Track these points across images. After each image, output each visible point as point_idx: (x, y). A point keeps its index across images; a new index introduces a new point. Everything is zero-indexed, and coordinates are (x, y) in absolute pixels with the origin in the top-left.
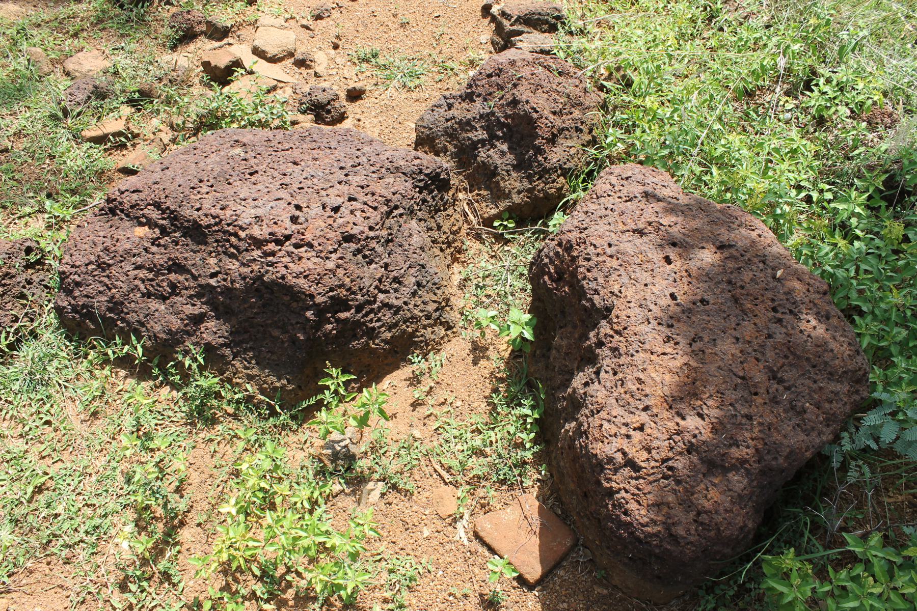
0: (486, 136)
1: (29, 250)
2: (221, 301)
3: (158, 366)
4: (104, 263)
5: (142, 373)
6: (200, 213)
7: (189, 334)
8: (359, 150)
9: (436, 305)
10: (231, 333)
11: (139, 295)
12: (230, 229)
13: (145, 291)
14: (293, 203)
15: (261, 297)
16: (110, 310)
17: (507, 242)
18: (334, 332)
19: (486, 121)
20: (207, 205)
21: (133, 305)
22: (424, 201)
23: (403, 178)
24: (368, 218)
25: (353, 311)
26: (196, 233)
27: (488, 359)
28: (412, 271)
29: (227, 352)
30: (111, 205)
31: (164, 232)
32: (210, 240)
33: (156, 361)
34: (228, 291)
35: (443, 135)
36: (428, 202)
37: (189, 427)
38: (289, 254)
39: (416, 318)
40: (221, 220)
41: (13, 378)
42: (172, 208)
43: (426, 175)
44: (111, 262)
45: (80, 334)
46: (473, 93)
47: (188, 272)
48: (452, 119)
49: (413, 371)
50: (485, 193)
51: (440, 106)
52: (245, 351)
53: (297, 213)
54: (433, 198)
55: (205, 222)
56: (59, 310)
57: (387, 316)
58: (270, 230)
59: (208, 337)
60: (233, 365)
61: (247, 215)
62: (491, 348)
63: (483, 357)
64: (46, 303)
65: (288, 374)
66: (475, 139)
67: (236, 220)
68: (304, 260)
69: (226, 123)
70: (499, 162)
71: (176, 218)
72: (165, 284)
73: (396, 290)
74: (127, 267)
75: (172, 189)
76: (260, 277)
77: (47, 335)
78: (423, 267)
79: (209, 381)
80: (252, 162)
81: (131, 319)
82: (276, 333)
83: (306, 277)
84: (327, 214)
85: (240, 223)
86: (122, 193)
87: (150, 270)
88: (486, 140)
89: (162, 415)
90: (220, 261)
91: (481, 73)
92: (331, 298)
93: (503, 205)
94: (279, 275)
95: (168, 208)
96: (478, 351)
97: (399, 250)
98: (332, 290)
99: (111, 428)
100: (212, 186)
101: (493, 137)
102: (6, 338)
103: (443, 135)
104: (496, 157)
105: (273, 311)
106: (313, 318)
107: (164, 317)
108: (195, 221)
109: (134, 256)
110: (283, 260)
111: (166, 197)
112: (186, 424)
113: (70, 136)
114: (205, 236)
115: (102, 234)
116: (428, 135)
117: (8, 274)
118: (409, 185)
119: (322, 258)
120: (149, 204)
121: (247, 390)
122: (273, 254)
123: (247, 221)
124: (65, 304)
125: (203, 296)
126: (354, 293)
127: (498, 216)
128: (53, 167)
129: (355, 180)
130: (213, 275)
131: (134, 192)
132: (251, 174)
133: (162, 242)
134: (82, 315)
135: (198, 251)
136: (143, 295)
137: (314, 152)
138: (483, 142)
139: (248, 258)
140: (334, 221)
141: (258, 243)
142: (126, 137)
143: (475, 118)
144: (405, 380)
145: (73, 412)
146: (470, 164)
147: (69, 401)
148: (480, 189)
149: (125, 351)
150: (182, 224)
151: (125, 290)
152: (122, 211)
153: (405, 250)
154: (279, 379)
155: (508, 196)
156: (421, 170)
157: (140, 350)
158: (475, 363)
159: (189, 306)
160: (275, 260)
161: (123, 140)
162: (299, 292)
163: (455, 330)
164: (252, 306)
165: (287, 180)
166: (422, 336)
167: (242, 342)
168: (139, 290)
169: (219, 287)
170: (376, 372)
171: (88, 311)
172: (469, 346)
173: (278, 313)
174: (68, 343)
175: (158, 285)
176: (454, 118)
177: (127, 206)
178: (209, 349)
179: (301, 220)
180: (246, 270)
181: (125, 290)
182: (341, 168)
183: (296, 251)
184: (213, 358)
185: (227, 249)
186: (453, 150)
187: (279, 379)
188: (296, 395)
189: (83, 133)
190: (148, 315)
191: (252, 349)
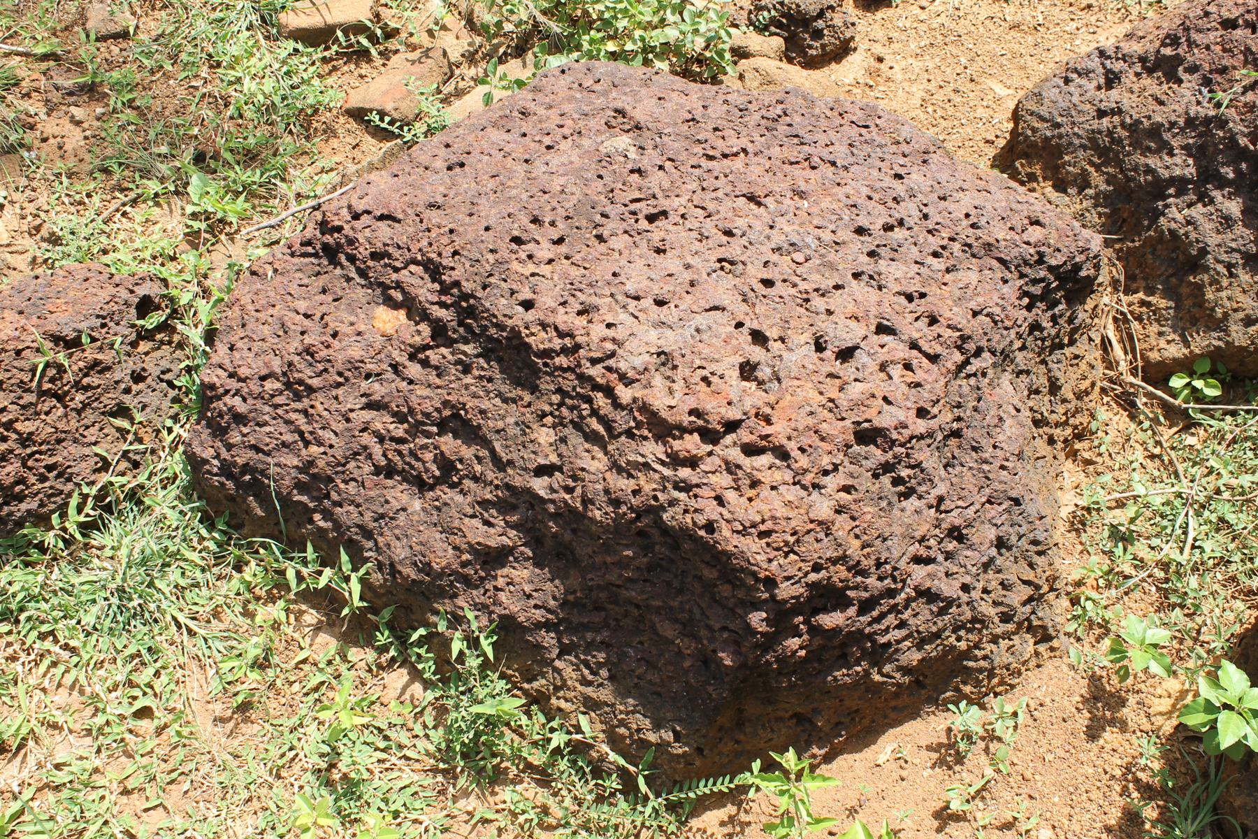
0: (1190, 172)
1: (145, 306)
2: (554, 534)
3: (391, 626)
4: (301, 382)
5: (357, 631)
6: (531, 316)
7: (467, 582)
8: (898, 176)
9: (1029, 591)
10: (564, 604)
11: (368, 468)
12: (596, 372)
13: (383, 463)
14: (748, 324)
15: (647, 549)
16: (301, 487)
17: (1189, 425)
18: (803, 653)
19: (1200, 135)
20: (547, 300)
21: (352, 488)
22: (1035, 327)
23: (1000, 272)
24: (918, 385)
25: (852, 611)
26: (515, 358)
27: (1123, 726)
28: (992, 511)
29: (548, 639)
30: (328, 239)
31: (440, 333)
32: (546, 384)
33: (386, 614)
34: (573, 518)
35: (1084, 147)
36: (1041, 329)
37: (440, 778)
38: (731, 468)
39: (982, 622)
40: (577, 347)
41: (84, 598)
42: (467, 286)
43: (1051, 269)
44: (315, 382)
45: (233, 515)
46: (1178, 60)
47: (486, 443)
48: (1113, 112)
49: (949, 730)
50: (1163, 303)
51: (1085, 73)
52: (589, 647)
53: (757, 354)
54: (1054, 319)
55: (540, 340)
56: (195, 463)
57: (921, 617)
58: (692, 403)
59: (510, 603)
60: (557, 670)
61: (640, 343)
62: (1132, 700)
63: (1112, 722)
64: (169, 423)
65: (680, 721)
66: (1165, 174)
67: (613, 354)
68: (765, 492)
69: (592, 42)
70: (1213, 240)
71: (471, 312)
72: (429, 456)
73: (949, 556)
74: (351, 400)
75: (471, 236)
76: (654, 511)
77: (164, 502)
78: (1017, 502)
79: (498, 699)
80: (656, 180)
81: (344, 518)
82: (668, 630)
83: (762, 535)
84: (826, 368)
85: (623, 366)
86: (356, 217)
87: (400, 418)
88: (1190, 181)
89: (386, 738)
90: (563, 440)
91: (1207, 14)
92: (812, 586)
93: (1201, 342)
94: (701, 519)
95: (457, 284)
96: (1104, 704)
97: (970, 459)
98: (817, 568)
99: (274, 752)
100: (560, 241)
101: (1208, 177)
102: (80, 510)
103: (1084, 147)
104: (1207, 226)
105: (669, 584)
106: (763, 628)
107: (420, 531)
108: (515, 333)
109: (368, 376)
110: (713, 479)
111: (455, 253)
112: (435, 771)
113: (254, 18)
114: (536, 372)
115: (302, 306)
116: (1047, 140)
117: (96, 363)
118: (1011, 291)
119: (804, 488)
120: (414, 262)
121: (578, 730)
122: (693, 462)
123: (639, 362)
124: (208, 453)
125: (513, 508)
126: (864, 573)
127: (1186, 366)
128: (215, 88)
129: (897, 273)
130: (541, 471)
131: (382, 218)
132: (651, 218)
133: (433, 356)
134: (239, 485)
135: (514, 401)
136: (378, 471)
137: (796, 171)
138: (1181, 184)
139: (632, 457)
140: (841, 389)
141: (663, 429)
142: (373, 39)
143: (1173, 124)
144: (929, 748)
145: (197, 693)
146: (1137, 229)
147: (194, 665)
148: (1150, 291)
149: (322, 582)
150: (485, 328)
151: (339, 453)
152: (352, 259)
153: (986, 462)
154: (657, 726)
155: (1219, 325)
156: (1041, 255)
157: (356, 587)
158: (1093, 733)
159: (476, 522)
160: (695, 480)
161: (365, 42)
162: (742, 570)
163: (1055, 643)
164: (624, 564)
165: (734, 249)
166: (985, 658)
167: (585, 627)
168: (370, 456)
169: (553, 501)
170: (866, 722)
171: (254, 479)
172: (1082, 687)
173: (680, 591)
174: (204, 532)
175: (412, 453)
176: (1119, 112)
177: (363, 252)
178: (507, 628)
179: (764, 372)
180: (623, 484)
181: (339, 453)
182: (860, 231)
183: (746, 462)
184: (515, 645)
185: (582, 417)
186: (1103, 187)
187: (657, 726)
188: (688, 764)
189: (283, 18)
190: (382, 516)
191: (605, 646)
